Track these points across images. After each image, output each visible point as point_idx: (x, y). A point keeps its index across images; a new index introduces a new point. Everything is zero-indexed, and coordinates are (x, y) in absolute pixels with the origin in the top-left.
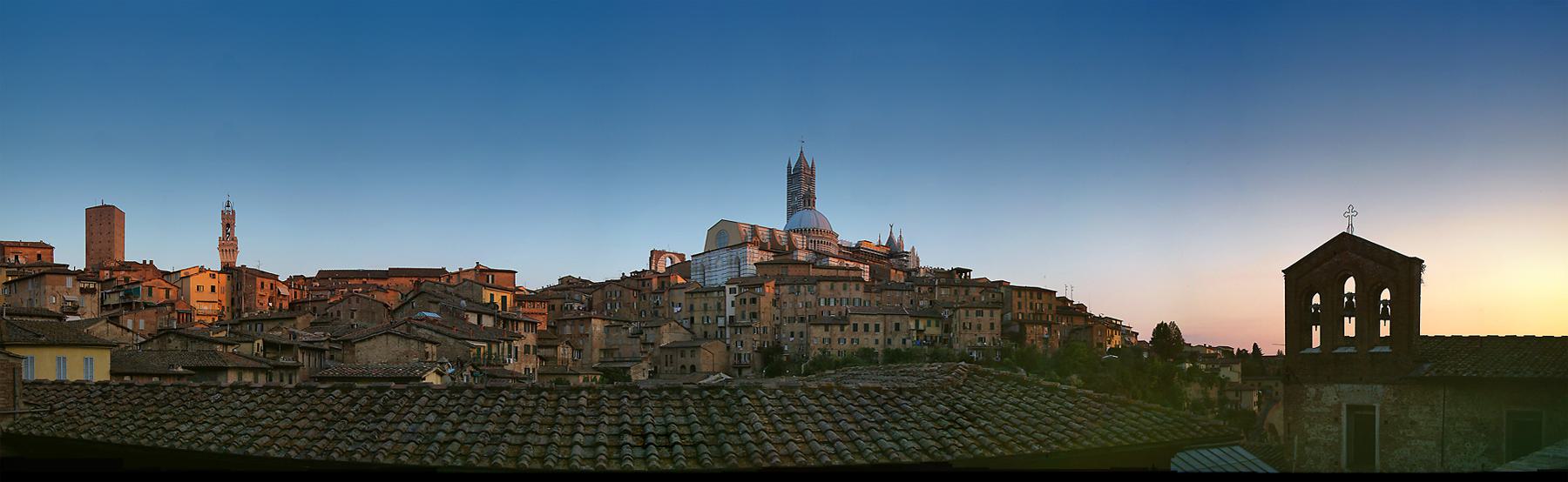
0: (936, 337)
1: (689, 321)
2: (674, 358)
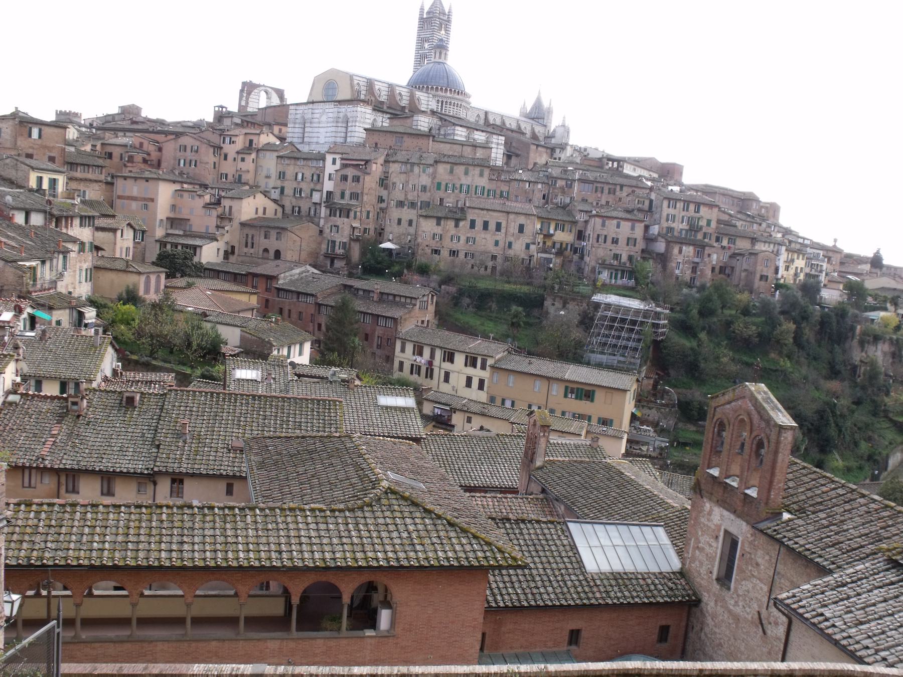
0: (567, 244)
1: (278, 191)
2: (256, 239)
